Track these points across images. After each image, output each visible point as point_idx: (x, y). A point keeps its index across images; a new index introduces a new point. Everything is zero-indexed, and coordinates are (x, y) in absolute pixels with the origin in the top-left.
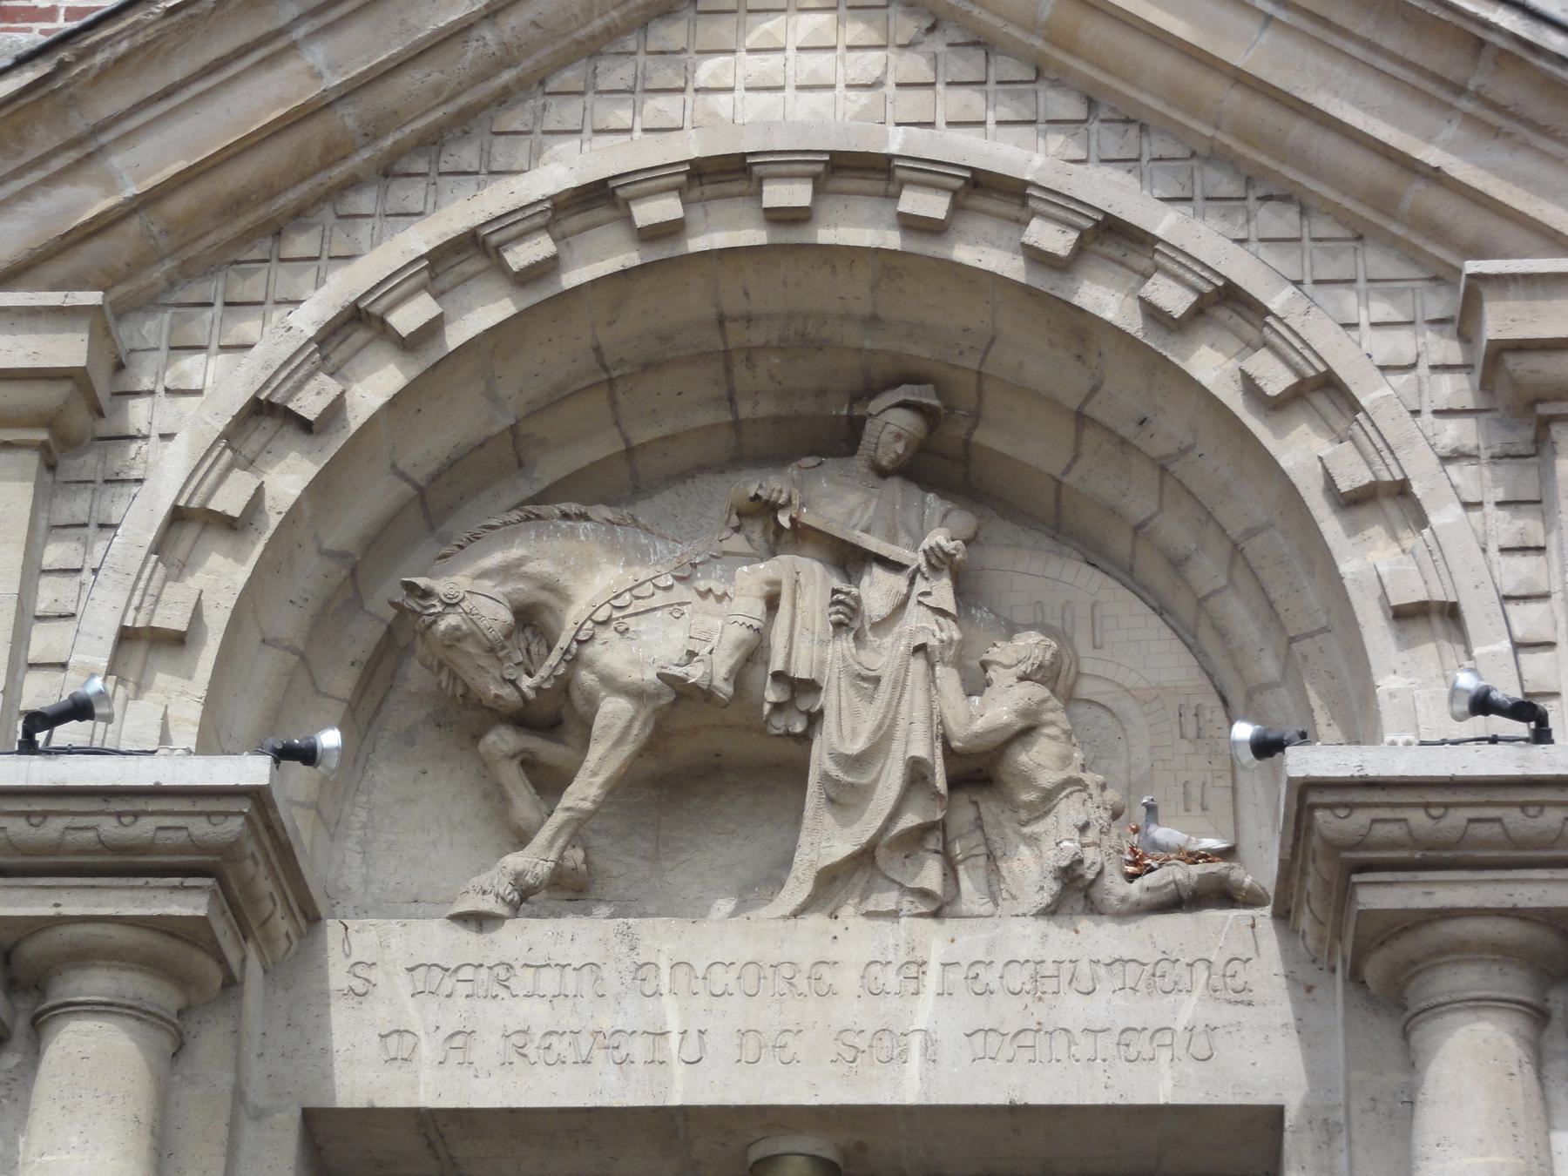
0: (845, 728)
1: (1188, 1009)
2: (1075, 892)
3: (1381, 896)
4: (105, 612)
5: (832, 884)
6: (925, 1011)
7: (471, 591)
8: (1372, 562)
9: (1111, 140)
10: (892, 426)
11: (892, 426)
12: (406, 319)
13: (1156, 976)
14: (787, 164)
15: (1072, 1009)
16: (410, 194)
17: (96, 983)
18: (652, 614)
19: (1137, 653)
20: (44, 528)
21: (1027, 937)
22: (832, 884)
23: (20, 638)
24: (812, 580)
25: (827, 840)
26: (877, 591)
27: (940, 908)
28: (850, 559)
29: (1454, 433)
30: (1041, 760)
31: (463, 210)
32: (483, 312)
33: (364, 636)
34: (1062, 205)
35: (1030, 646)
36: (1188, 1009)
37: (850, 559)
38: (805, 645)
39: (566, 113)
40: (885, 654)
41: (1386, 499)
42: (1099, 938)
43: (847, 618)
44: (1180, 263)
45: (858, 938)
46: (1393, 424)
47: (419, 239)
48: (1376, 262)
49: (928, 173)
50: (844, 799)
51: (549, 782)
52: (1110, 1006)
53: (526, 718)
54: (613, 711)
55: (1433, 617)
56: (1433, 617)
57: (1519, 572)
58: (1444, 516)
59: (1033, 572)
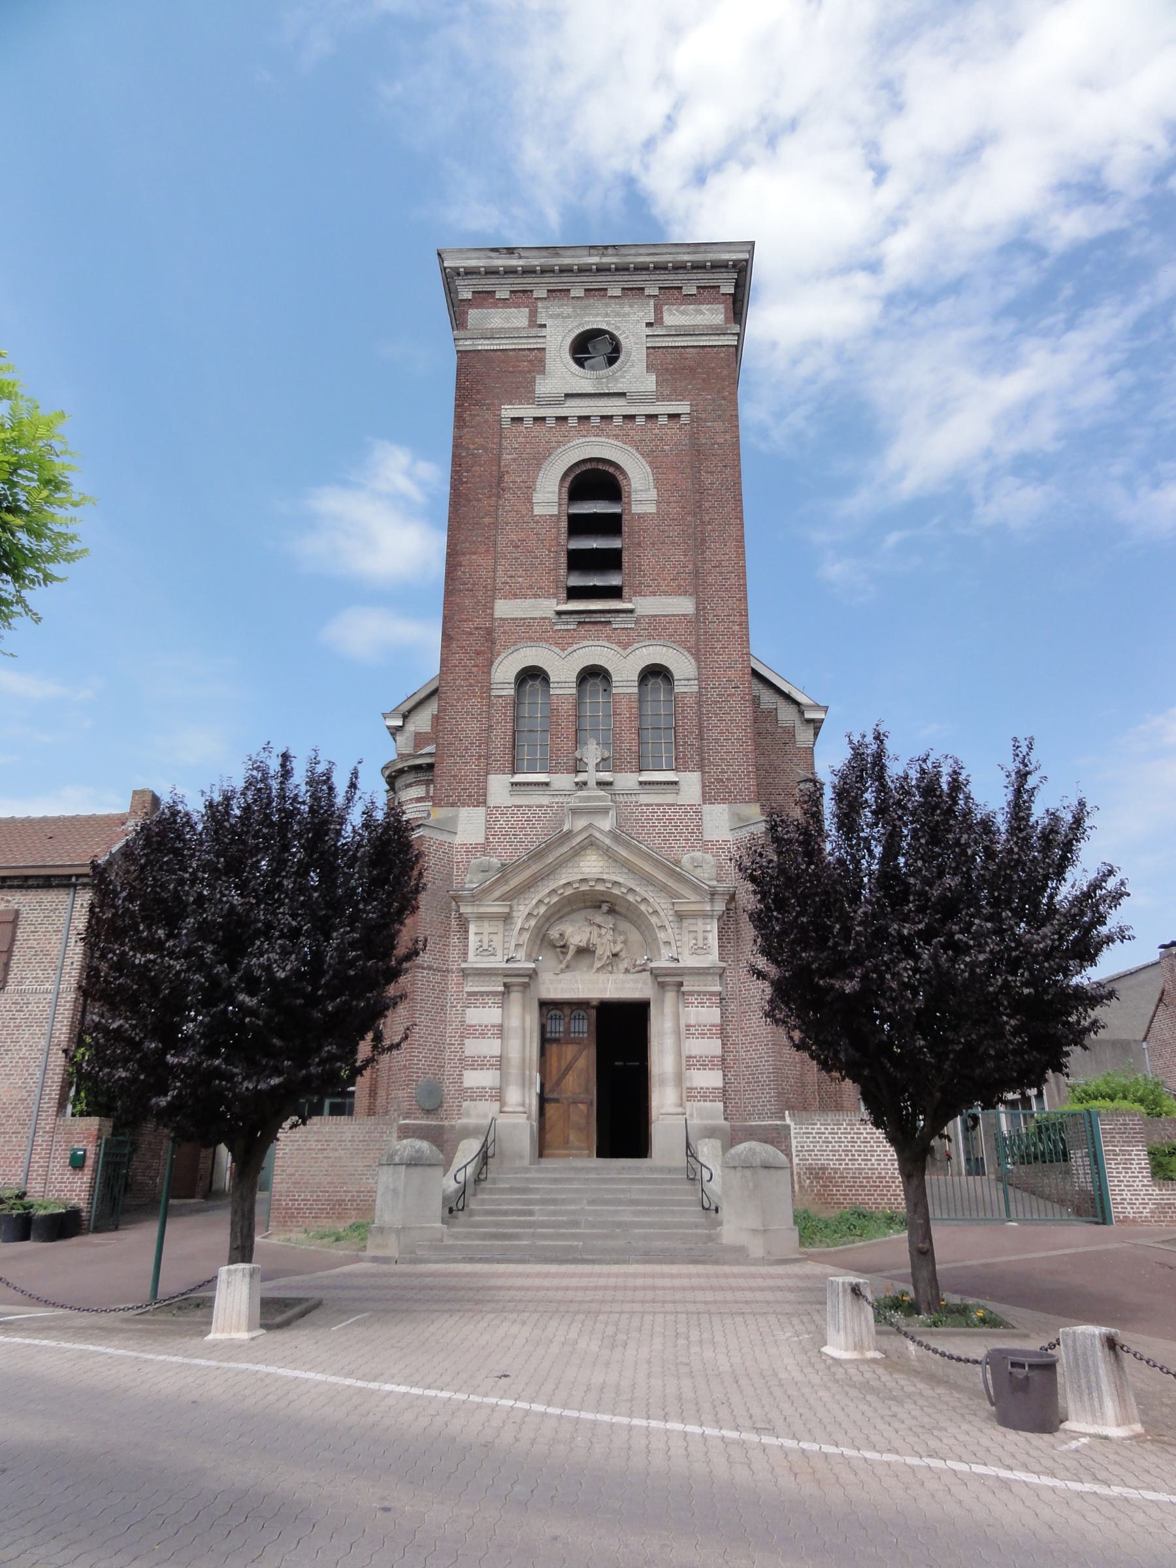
0: (599, 952)
1: (640, 985)
2: (627, 971)
3: (660, 979)
4: (513, 944)
5: (598, 969)
6: (609, 986)
7: (554, 933)
8: (662, 936)
9: (631, 876)
10: (605, 907)
11: (605, 907)
12: (546, 901)
13: (636, 981)
14: (592, 880)
15: (627, 985)
16: (546, 883)
17: (515, 988)
18: (576, 933)
19: (635, 936)
20: (505, 930)
21: (621, 976)
22: (598, 969)
23: (450, 290)
24: (596, 930)
25: (598, 964)
26: (603, 931)
27: (611, 973)
28: (600, 926)
29: (671, 919)
30: (623, 954)
31: (552, 885)
32: (555, 899)
33: (541, 936)
34: (625, 886)
35: (622, 938)
36: (640, 985)
37: (600, 926)
38: (595, 940)
39: (564, 871)
40: (604, 940)
41: (662, 927)
42: (630, 976)
43: (600, 936)
44: (639, 895)
45: (602, 977)
46: (664, 918)
47: (547, 891)
48: (663, 894)
49: (609, 881)
50: (600, 959)
51: (565, 954)
52: (631, 985)
53: (563, 946)
54: (572, 947)
55: (667, 943)
56: (667, 943)
57: (677, 937)
58: (670, 930)
59: (624, 925)
